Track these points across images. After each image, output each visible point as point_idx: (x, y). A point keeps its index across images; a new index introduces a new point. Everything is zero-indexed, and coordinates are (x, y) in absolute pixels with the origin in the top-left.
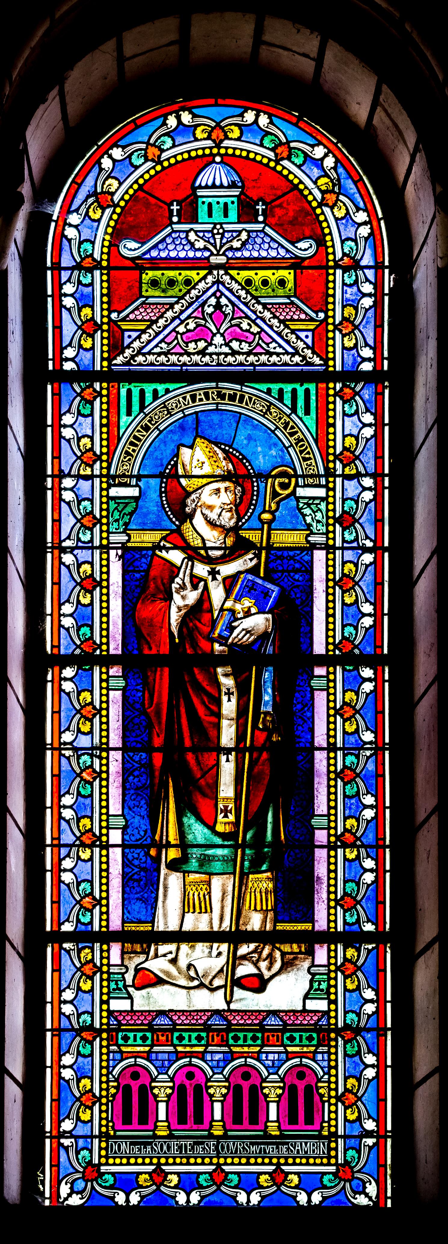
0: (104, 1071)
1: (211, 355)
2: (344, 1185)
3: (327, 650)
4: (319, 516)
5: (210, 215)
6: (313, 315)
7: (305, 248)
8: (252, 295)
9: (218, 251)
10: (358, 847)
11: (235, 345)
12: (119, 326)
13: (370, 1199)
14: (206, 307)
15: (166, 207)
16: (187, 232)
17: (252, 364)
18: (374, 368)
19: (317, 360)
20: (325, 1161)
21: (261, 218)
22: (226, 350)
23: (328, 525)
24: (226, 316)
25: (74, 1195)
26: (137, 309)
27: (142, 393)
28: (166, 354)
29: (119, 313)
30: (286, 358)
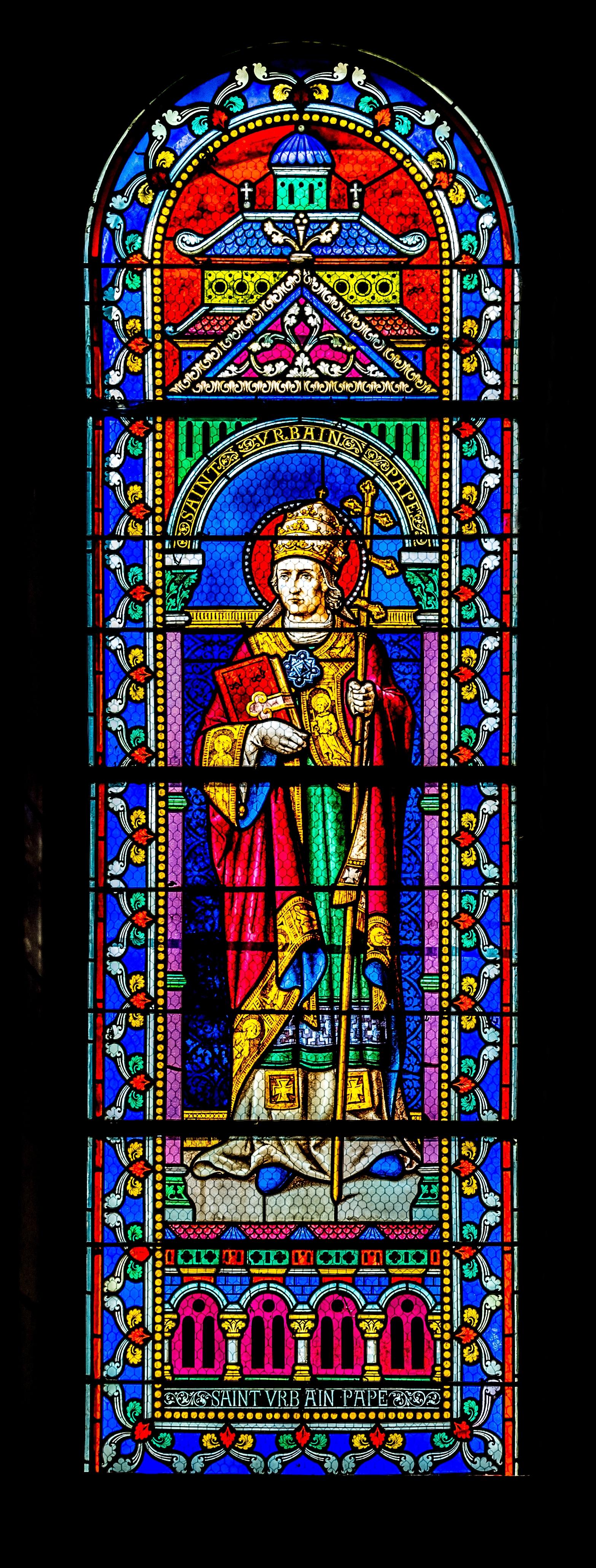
0: (159, 1300)
1: (292, 380)
2: (461, 1446)
3: (440, 760)
4: (430, 588)
5: (291, 201)
6: (424, 329)
7: (413, 244)
8: (345, 302)
9: (301, 248)
10: (478, 1015)
11: (323, 367)
12: (176, 344)
13: (110, 1464)
14: (286, 318)
15: (236, 189)
16: (263, 223)
17: (345, 393)
18: (501, 395)
19: (428, 388)
20: (436, 1416)
21: (356, 205)
22: (311, 373)
23: (441, 598)
24: (312, 329)
25: (121, 1460)
26: (199, 319)
27: (206, 428)
28: (236, 379)
29: (175, 326)
30: (387, 385)
